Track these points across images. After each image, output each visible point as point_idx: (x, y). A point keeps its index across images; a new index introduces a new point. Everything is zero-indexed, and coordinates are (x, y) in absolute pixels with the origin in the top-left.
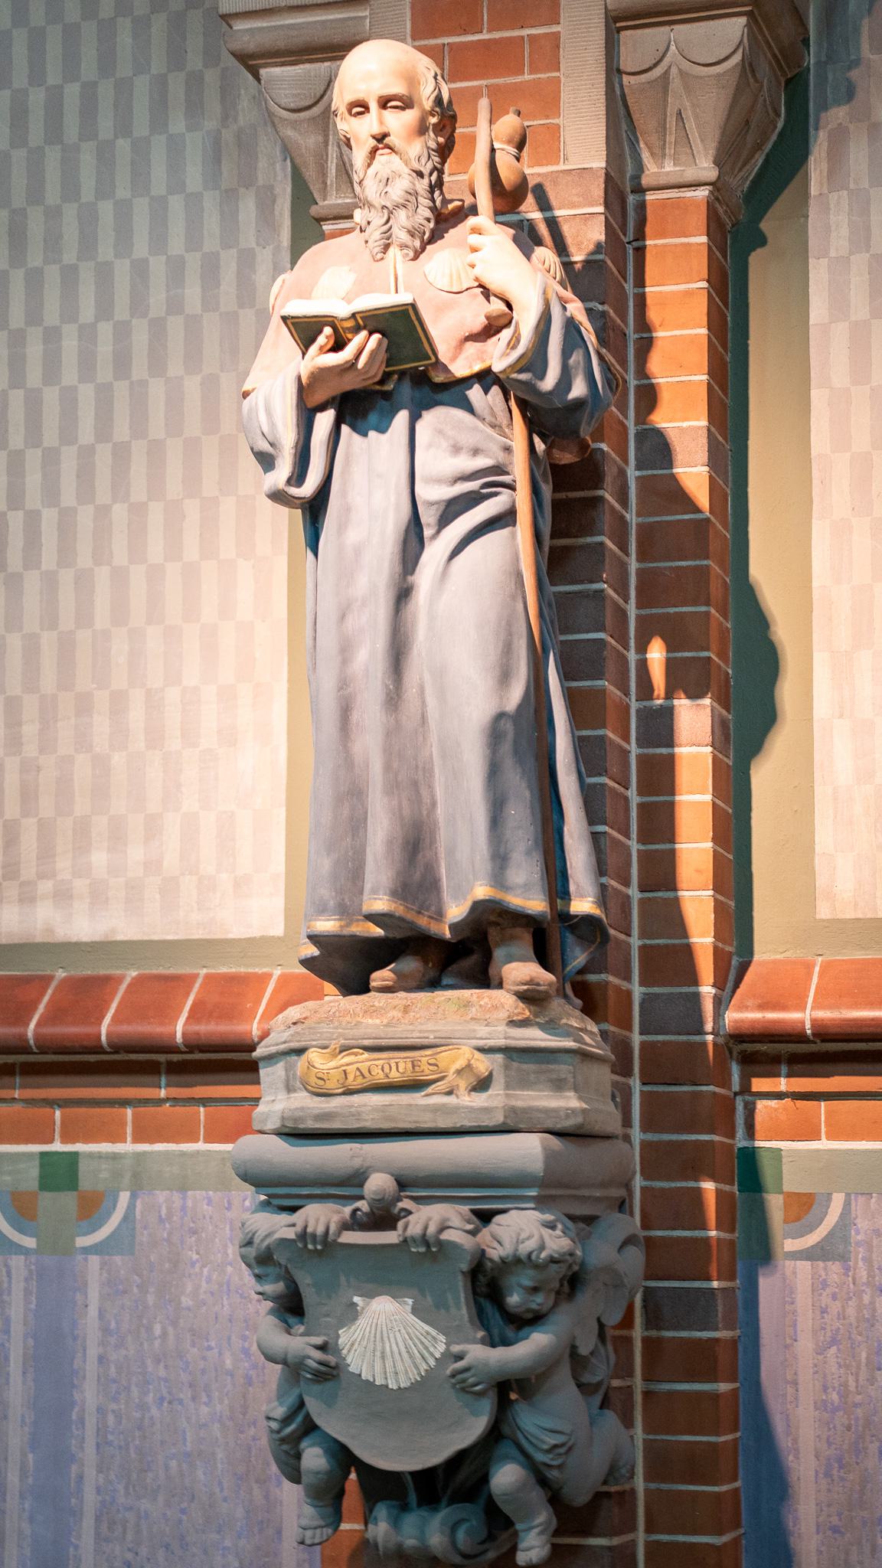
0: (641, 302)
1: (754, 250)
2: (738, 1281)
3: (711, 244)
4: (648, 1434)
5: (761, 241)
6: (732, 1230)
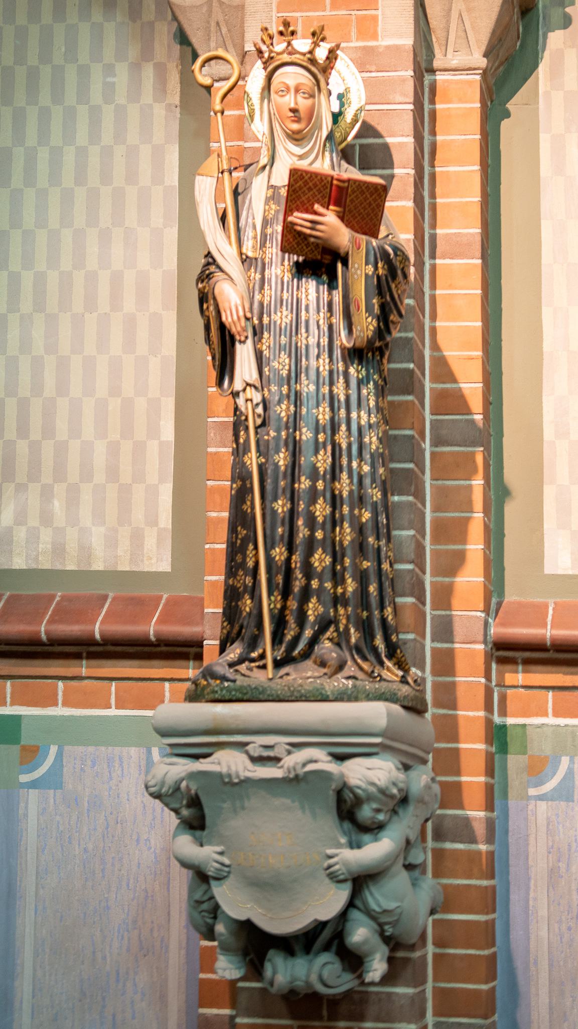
0: (433, 330)
1: (503, 120)
2: (495, 813)
3: (487, 583)
4: (433, 383)
5: (508, 115)
6: (492, 810)
